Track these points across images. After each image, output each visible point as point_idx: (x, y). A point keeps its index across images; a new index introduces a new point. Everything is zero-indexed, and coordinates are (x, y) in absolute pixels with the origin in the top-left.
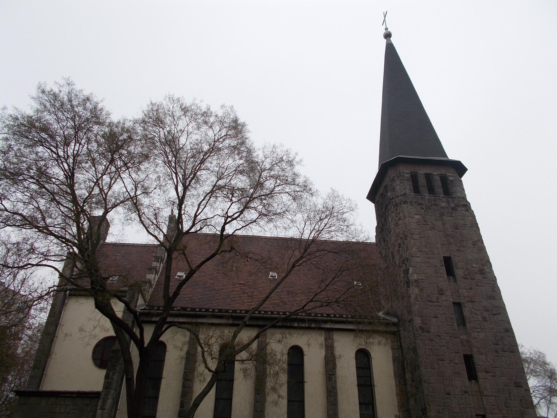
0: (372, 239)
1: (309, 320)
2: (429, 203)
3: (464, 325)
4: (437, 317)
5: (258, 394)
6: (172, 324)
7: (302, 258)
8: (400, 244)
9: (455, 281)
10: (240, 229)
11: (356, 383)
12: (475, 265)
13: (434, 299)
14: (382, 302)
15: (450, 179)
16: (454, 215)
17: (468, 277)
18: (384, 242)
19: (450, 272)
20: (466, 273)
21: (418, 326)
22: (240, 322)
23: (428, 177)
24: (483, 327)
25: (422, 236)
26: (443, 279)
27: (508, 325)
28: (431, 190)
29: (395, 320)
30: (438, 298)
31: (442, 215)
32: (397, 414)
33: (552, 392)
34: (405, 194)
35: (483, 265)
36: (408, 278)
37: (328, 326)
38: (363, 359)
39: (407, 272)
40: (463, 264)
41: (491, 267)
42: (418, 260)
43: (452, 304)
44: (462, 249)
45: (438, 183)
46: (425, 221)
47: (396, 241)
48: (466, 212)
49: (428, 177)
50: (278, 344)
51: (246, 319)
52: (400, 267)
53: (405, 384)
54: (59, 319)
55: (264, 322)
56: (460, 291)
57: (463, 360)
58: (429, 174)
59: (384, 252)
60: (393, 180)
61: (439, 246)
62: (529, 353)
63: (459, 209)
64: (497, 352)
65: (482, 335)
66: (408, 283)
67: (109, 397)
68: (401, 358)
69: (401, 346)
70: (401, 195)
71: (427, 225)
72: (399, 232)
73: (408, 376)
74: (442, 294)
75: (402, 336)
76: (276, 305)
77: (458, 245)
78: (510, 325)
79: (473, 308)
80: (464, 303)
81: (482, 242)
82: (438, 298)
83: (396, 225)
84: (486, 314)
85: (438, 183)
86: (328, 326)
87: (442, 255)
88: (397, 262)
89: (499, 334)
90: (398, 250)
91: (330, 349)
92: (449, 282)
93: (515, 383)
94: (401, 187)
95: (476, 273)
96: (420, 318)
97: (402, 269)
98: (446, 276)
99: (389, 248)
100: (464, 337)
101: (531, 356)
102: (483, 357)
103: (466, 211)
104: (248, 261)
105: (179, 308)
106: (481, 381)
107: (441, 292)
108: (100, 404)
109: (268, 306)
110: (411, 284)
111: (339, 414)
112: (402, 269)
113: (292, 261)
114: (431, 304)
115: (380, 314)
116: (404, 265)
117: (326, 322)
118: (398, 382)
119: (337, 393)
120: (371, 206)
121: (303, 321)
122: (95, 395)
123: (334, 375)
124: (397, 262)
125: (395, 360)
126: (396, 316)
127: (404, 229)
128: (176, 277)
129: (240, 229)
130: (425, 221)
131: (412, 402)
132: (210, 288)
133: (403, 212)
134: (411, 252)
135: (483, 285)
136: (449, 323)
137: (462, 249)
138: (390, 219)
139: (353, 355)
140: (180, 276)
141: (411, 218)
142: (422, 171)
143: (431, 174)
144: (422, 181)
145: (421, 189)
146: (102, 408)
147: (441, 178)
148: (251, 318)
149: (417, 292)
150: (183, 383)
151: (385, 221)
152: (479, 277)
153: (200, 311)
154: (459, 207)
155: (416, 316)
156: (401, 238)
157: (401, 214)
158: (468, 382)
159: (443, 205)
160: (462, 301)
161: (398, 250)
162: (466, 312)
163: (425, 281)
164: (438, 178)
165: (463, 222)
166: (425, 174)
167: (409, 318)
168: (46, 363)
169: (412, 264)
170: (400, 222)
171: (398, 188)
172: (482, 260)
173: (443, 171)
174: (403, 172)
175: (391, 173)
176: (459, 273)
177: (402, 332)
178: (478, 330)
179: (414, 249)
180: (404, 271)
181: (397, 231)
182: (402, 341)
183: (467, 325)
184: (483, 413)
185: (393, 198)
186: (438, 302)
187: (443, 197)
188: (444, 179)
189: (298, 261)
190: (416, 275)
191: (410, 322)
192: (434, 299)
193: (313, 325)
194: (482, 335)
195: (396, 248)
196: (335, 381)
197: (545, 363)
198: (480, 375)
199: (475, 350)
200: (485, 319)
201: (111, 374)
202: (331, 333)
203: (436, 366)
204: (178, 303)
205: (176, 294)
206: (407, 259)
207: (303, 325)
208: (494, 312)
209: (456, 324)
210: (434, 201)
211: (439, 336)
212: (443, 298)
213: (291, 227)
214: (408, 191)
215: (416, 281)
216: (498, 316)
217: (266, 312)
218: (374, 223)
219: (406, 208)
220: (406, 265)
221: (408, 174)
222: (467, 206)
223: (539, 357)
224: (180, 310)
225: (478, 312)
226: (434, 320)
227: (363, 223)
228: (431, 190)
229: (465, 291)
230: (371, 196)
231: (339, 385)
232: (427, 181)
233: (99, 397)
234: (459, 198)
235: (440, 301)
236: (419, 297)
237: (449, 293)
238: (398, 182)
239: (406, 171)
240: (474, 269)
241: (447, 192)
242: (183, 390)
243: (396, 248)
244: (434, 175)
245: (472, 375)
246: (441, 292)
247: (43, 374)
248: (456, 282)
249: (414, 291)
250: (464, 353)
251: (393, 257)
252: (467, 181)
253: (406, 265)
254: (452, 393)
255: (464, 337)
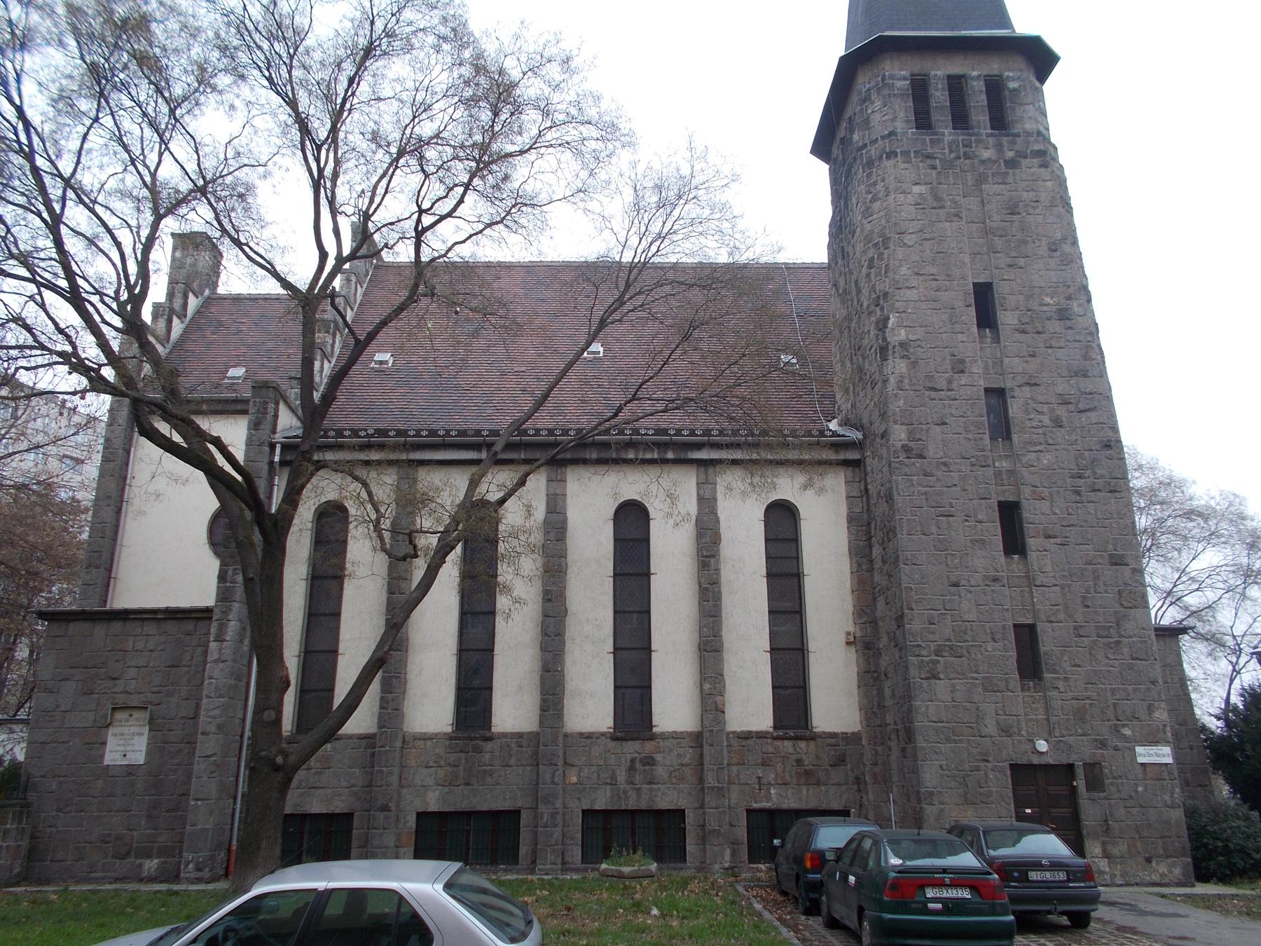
0: (820, 255)
1: (658, 445)
2: (951, 151)
3: (1008, 436)
4: (945, 424)
5: (549, 600)
6: (320, 465)
7: (620, 302)
8: (872, 260)
9: (997, 339)
10: (464, 242)
11: (764, 572)
12: (1048, 300)
13: (943, 384)
14: (838, 396)
15: (1012, 85)
16: (1010, 179)
17: (1028, 328)
18: (843, 258)
19: (986, 316)
20: (1025, 320)
21: (900, 444)
22: (484, 455)
23: (956, 85)
24: (1050, 441)
25: (926, 236)
26: (966, 336)
27: (1111, 434)
28: (960, 119)
29: (855, 435)
30: (950, 381)
31: (981, 180)
32: (851, 629)
33: (1249, 575)
34: (892, 133)
35: (1069, 298)
36: (884, 339)
37: (703, 455)
38: (782, 520)
39: (882, 325)
40: (1021, 298)
41: (1089, 301)
42: (912, 294)
43: (982, 393)
44: (1022, 262)
45: (978, 99)
46: (937, 198)
47: (864, 252)
48: (1042, 170)
49: (956, 85)
50: (592, 500)
51: (498, 447)
52: (870, 314)
53: (871, 570)
54: (127, 465)
55: (562, 454)
56: (1007, 361)
57: (997, 514)
58: (960, 78)
59: (842, 282)
60: (866, 99)
61: (967, 260)
62: (1206, 498)
63: (1025, 162)
64: (1078, 493)
65: (1046, 459)
66: (884, 351)
67: (230, 617)
68: (865, 516)
69: (866, 490)
70: (883, 137)
71: (943, 207)
72: (872, 231)
73: (877, 551)
74: (962, 372)
75: (869, 469)
76: (571, 413)
77: (1014, 254)
78: (1118, 432)
79: (1032, 399)
80: (1012, 389)
81: (1075, 242)
82: (950, 381)
83: (867, 213)
84: (1061, 411)
85: (978, 99)
86: (703, 455)
87: (970, 280)
88: (865, 305)
89: (1087, 454)
90: (868, 275)
91: (707, 505)
92: (981, 342)
93: (1111, 556)
94: (886, 114)
95: (1049, 319)
96: (904, 427)
97: (873, 319)
98: (975, 329)
99: (851, 273)
100: (1005, 464)
101: (1212, 503)
102: (1044, 506)
103: (1041, 166)
104: (457, 313)
105: (371, 432)
106: (1032, 556)
107: (959, 367)
108: (213, 630)
109: (543, 420)
110: (890, 352)
111: (723, 633)
112: (873, 319)
113: (599, 313)
114: (933, 394)
115: (833, 425)
116: (878, 309)
117: (699, 446)
118: (855, 566)
119: (720, 593)
120: (821, 169)
121: (606, 445)
122: (203, 614)
123: (714, 556)
124: (865, 305)
125: (851, 520)
126: (858, 427)
127: (883, 222)
128: (373, 365)
129: (464, 242)
130: (937, 198)
131: (881, 605)
132: (395, 380)
133: (883, 180)
134: (897, 277)
135: (1062, 344)
136: (970, 436)
137: (1022, 262)
138: (854, 201)
139: (760, 513)
140: (381, 363)
141: (904, 192)
142: (940, 69)
143: (962, 76)
144: (939, 96)
145: (935, 116)
146: (220, 639)
147: (987, 86)
148: (509, 446)
149: (904, 370)
150: (389, 584)
151: (846, 206)
152: (1054, 326)
153: (418, 435)
154: (1026, 157)
155: (895, 423)
156: (876, 245)
157: (880, 186)
158: (1003, 559)
159: (987, 154)
160: (1009, 384)
161: (868, 275)
162: (1015, 409)
163: (923, 344)
164: (979, 85)
165: (1032, 194)
166: (949, 77)
167: (882, 429)
168: (113, 554)
169: (898, 305)
170: (877, 205)
171: (876, 118)
172: (1069, 286)
173: (994, 65)
174: (892, 77)
175: (864, 81)
176: (1007, 319)
177: (869, 461)
178: (1038, 448)
179: (904, 270)
180: (877, 322)
181: (868, 227)
182: (869, 480)
183: (1015, 437)
184: (1030, 622)
185: (865, 146)
186: (950, 390)
187: (988, 135)
188: (995, 88)
189: (611, 310)
190: (903, 332)
191: (883, 437)
192: (943, 384)
193: (670, 455)
194: (1046, 459)
195: (864, 270)
196: (718, 570)
197: (1243, 518)
198: (1032, 543)
199: (1027, 491)
200: (1058, 423)
201: (230, 572)
202: (711, 470)
203: (934, 529)
204: (338, 418)
205: (329, 398)
206: (886, 294)
207: (648, 456)
208: (1081, 406)
209: (987, 437)
210: (964, 146)
211: (945, 464)
212: (964, 379)
213: (573, 232)
214: (900, 126)
215: (903, 345)
216: (1089, 414)
217: (538, 431)
218: (824, 211)
219: (892, 169)
220: (882, 309)
221: (905, 79)
222: (1046, 155)
223: (1231, 505)
224: (372, 436)
225: (1045, 408)
226: (938, 429)
227: (783, 215)
228: (960, 119)
229: (1016, 360)
230: (822, 147)
231: (727, 574)
232: (950, 96)
233: (211, 618)
234: (1029, 134)
235: (954, 385)
236: (906, 381)
237: (977, 369)
238: (878, 104)
239: (898, 71)
240: (1045, 308)
241: (999, 121)
242: (388, 598)
243: (864, 270)
244: (972, 78)
245: (1014, 543)
246: (959, 367)
247: (110, 578)
248: (998, 342)
249: (897, 367)
250: (1001, 499)
251: (859, 291)
252: (1054, 88)
253: (882, 309)
254: (964, 582)
255: (1005, 464)
